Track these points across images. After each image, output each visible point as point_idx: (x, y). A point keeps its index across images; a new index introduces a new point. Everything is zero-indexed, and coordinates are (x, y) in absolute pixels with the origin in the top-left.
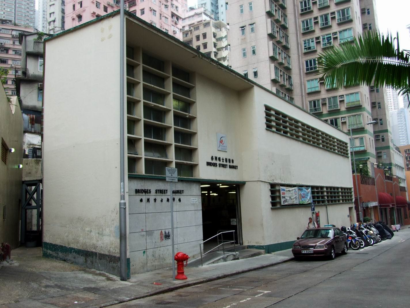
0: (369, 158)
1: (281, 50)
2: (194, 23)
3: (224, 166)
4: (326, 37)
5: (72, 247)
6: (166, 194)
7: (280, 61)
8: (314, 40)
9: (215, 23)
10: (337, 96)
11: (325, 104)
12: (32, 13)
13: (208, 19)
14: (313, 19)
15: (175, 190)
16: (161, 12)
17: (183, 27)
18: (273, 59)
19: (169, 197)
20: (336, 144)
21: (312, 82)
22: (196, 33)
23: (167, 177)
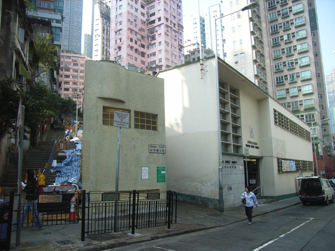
0: (319, 142)
3: (253, 147)
4: (290, 62)
5: (183, 193)
7: (261, 77)
8: (282, 63)
10: (298, 101)
11: (290, 106)
14: (281, 50)
16: (172, 44)
19: (231, 165)
23: (128, 123)
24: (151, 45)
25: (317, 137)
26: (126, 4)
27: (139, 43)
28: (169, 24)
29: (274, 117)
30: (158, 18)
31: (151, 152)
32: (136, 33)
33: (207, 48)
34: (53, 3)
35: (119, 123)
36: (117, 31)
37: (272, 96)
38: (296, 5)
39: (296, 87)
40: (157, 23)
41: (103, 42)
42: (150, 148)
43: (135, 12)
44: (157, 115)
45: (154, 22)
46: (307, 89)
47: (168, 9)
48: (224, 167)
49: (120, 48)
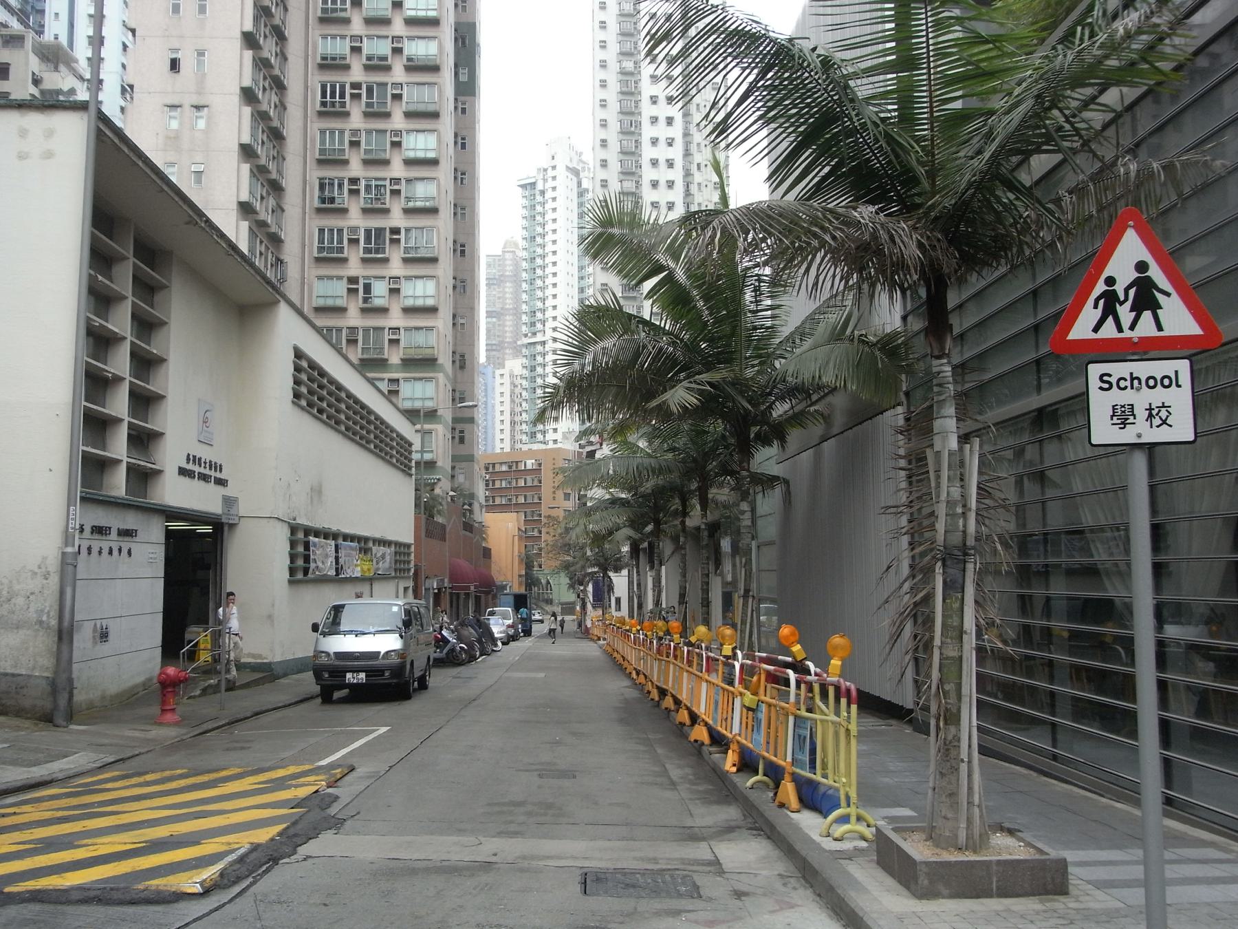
0: (439, 480)
3: (204, 478)
4: (373, 183)
7: (261, 216)
11: (356, 341)
21: (330, 282)
25: (436, 411)
29: (294, 376)
33: (48, 37)
37: (295, 298)
38: (415, 379)
39: (387, 37)
46: (419, 292)
48: (84, 551)
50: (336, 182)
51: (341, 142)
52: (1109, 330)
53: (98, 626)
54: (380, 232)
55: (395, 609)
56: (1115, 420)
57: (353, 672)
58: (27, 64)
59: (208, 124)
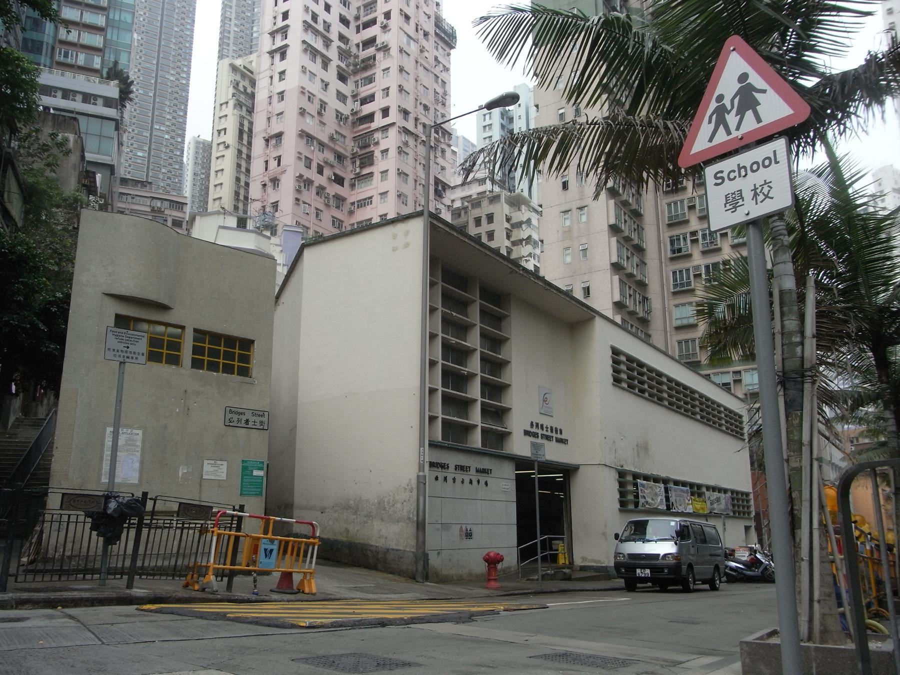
1: (631, 253)
2: (471, 196)
6: (468, 473)
7: (629, 270)
9: (510, 197)
11: (700, 275)
12: (177, 167)
13: (497, 189)
15: (890, 258)
17: (453, 201)
18: (616, 267)
19: (472, 477)
20: (723, 415)
22: (476, 213)
24: (361, 178)
26: (298, 69)
27: (327, 172)
28: (410, 126)
30: (380, 109)
31: (231, 424)
32: (322, 145)
34: (101, 54)
35: (120, 353)
36: (272, 137)
40: (379, 121)
41: (238, 164)
42: (229, 416)
43: (322, 91)
44: (253, 342)
45: (370, 117)
47: (409, 86)
49: (275, 181)
50: (681, 237)
51: (683, 209)
52: (721, 136)
53: (464, 528)
54: (715, 265)
55: (673, 524)
56: (728, 207)
57: (641, 568)
58: (502, 210)
59: (588, 218)
